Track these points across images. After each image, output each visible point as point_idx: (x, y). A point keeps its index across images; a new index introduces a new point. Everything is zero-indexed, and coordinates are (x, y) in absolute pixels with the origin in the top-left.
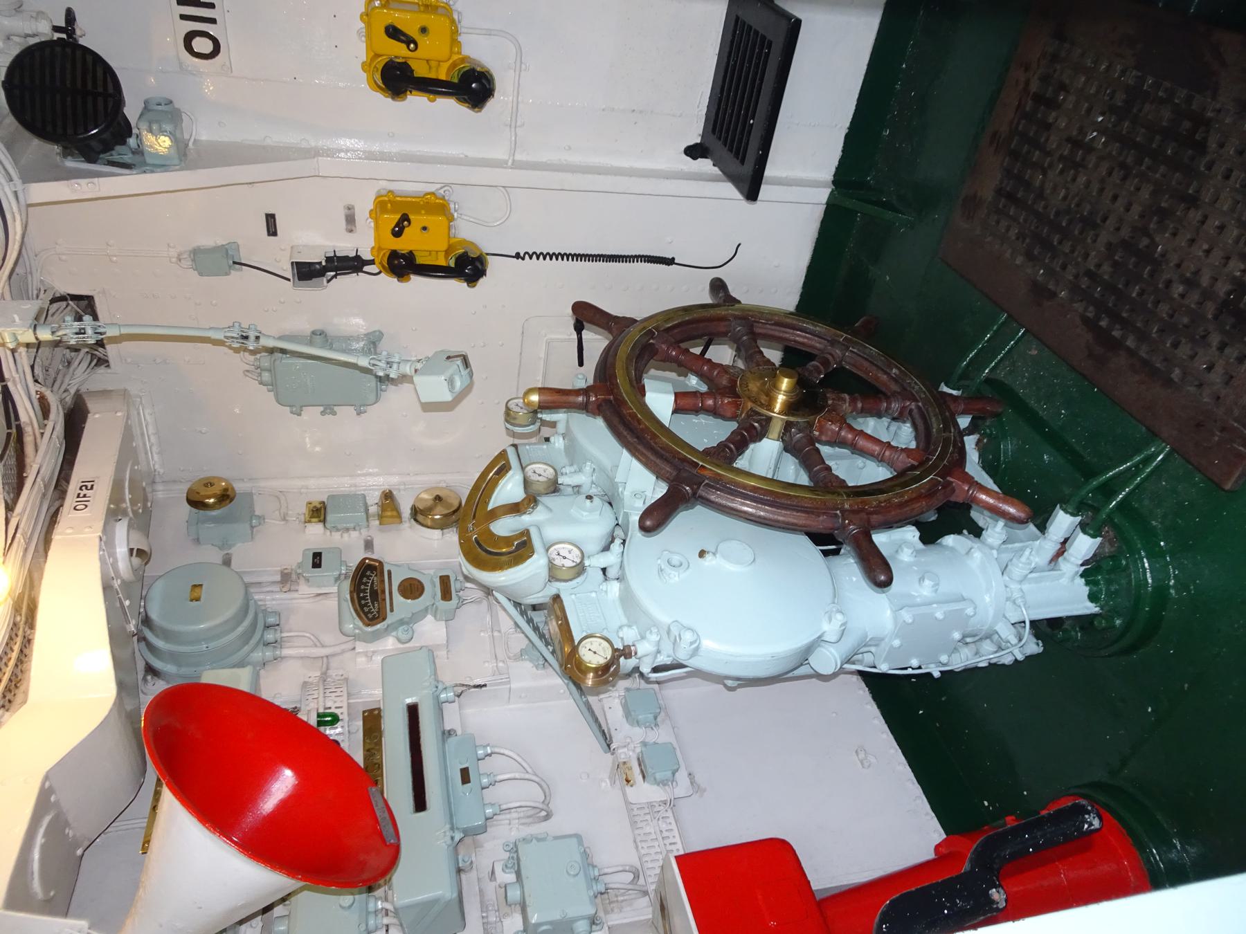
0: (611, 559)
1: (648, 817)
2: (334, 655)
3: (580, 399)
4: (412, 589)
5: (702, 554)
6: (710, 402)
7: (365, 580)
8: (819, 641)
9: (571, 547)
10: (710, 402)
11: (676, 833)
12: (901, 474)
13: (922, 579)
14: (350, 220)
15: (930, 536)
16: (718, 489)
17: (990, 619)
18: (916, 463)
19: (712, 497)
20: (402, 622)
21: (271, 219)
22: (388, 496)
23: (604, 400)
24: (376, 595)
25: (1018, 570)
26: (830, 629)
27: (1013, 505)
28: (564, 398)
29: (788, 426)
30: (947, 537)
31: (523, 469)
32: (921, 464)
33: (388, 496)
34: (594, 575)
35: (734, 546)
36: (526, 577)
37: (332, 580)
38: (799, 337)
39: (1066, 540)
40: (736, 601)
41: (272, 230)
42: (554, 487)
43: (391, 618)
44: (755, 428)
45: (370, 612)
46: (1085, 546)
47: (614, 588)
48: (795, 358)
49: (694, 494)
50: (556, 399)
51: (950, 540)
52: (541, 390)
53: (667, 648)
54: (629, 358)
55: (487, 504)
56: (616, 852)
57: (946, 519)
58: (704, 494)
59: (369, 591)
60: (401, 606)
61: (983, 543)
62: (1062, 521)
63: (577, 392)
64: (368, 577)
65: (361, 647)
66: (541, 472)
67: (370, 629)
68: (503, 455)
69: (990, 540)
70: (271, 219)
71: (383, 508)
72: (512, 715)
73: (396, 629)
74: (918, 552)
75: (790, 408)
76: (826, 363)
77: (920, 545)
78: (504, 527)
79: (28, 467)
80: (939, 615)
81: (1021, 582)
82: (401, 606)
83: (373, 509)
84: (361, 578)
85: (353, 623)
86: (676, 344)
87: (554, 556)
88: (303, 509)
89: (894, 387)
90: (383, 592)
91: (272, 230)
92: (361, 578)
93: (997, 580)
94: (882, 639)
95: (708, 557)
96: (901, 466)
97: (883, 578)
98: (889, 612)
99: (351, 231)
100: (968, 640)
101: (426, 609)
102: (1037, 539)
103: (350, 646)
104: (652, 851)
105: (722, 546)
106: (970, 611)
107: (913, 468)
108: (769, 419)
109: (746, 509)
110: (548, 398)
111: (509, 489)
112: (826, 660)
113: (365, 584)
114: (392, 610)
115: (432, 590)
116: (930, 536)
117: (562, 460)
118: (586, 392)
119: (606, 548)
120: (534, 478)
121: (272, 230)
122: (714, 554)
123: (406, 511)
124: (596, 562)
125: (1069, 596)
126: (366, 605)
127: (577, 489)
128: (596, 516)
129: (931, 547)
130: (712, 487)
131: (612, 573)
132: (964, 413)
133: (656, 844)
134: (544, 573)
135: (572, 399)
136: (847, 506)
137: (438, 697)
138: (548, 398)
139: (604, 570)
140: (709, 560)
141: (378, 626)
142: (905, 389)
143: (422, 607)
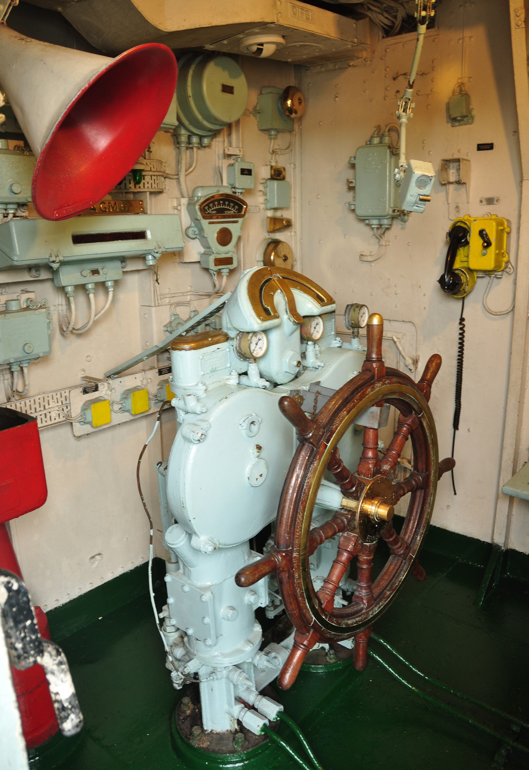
0: (254, 378)
1: (60, 404)
2: (179, 182)
3: (374, 356)
4: (224, 237)
5: (259, 448)
6: (370, 454)
7: (232, 204)
8: (190, 534)
9: (264, 349)
10: (370, 454)
11: (49, 423)
12: (316, 595)
13: (232, 608)
14: (490, 201)
15: (260, 614)
16: (309, 457)
17: (201, 655)
18: (323, 606)
19: (303, 453)
20: (201, 230)
21: (489, 147)
22: (288, 225)
23: (374, 373)
24: (221, 212)
25: (235, 675)
26: (202, 541)
27: (291, 676)
28: (375, 344)
29: (352, 513)
30: (260, 627)
31: (320, 316)
32: (323, 610)
33: (288, 225)
34: (243, 366)
35: (263, 470)
36: (244, 314)
37: (232, 183)
38: (412, 525)
39: (256, 710)
40: (226, 467)
41: (481, 147)
42: (304, 339)
43: (205, 223)
44: (352, 488)
45: (209, 207)
46: (255, 724)
47: (233, 380)
48: (397, 522)
49: (307, 440)
50: (375, 338)
51: (258, 629)
52: (381, 326)
53: (189, 418)
54: (402, 394)
55: (296, 287)
56: (37, 379)
57: (272, 629)
58: (306, 447)
59: (225, 207)
60: (212, 230)
61: (257, 653)
62: (272, 709)
63: (379, 353)
64: (233, 207)
65: (184, 201)
66: (317, 329)
67: (197, 207)
68: (331, 301)
69: (258, 657)
70: (489, 147)
71: (281, 220)
72: (133, 315)
73: (196, 226)
74: (250, 605)
75: (365, 515)
76: (395, 542)
77: (255, 608)
78: (279, 299)
79: (186, 209)
80: (207, 620)
81: (228, 678)
82: (212, 230)
83: (279, 214)
84: (233, 202)
85: (201, 195)
86: (411, 432)
87: (259, 336)
88: (280, 165)
89: (376, 591)
90: (224, 217)
91: (482, 147)
92: (233, 202)
93: (229, 662)
94: (189, 578)
95: (256, 450)
96: (321, 596)
97: (243, 579)
98: (209, 583)
99: (481, 202)
100: (186, 639)
101: (209, 248)
102: (256, 689)
103: (185, 194)
104: (37, 406)
105: (262, 462)
106: (209, 642)
107: (320, 604)
108: (357, 499)
109: (294, 479)
110: (376, 331)
111: (307, 305)
112: (175, 538)
113: (229, 205)
114: (210, 223)
115: (224, 251)
116: (260, 614)
117: (323, 345)
118: (380, 360)
119: (262, 376)
120: (314, 324)
121: (481, 147)
122: (258, 457)
123: (278, 236)
124: (253, 369)
125: (218, 714)
126: (214, 205)
127: (304, 355)
128: (286, 369)
129: (253, 615)
130: (311, 454)
131: (244, 379)
132: (357, 643)
133: (42, 408)
134: (246, 328)
135: (375, 350)
136: (295, 555)
137: (150, 254)
138: (376, 331)
139: (246, 374)
140: (253, 451)
141: (199, 213)
142: (375, 600)
143: (211, 245)
